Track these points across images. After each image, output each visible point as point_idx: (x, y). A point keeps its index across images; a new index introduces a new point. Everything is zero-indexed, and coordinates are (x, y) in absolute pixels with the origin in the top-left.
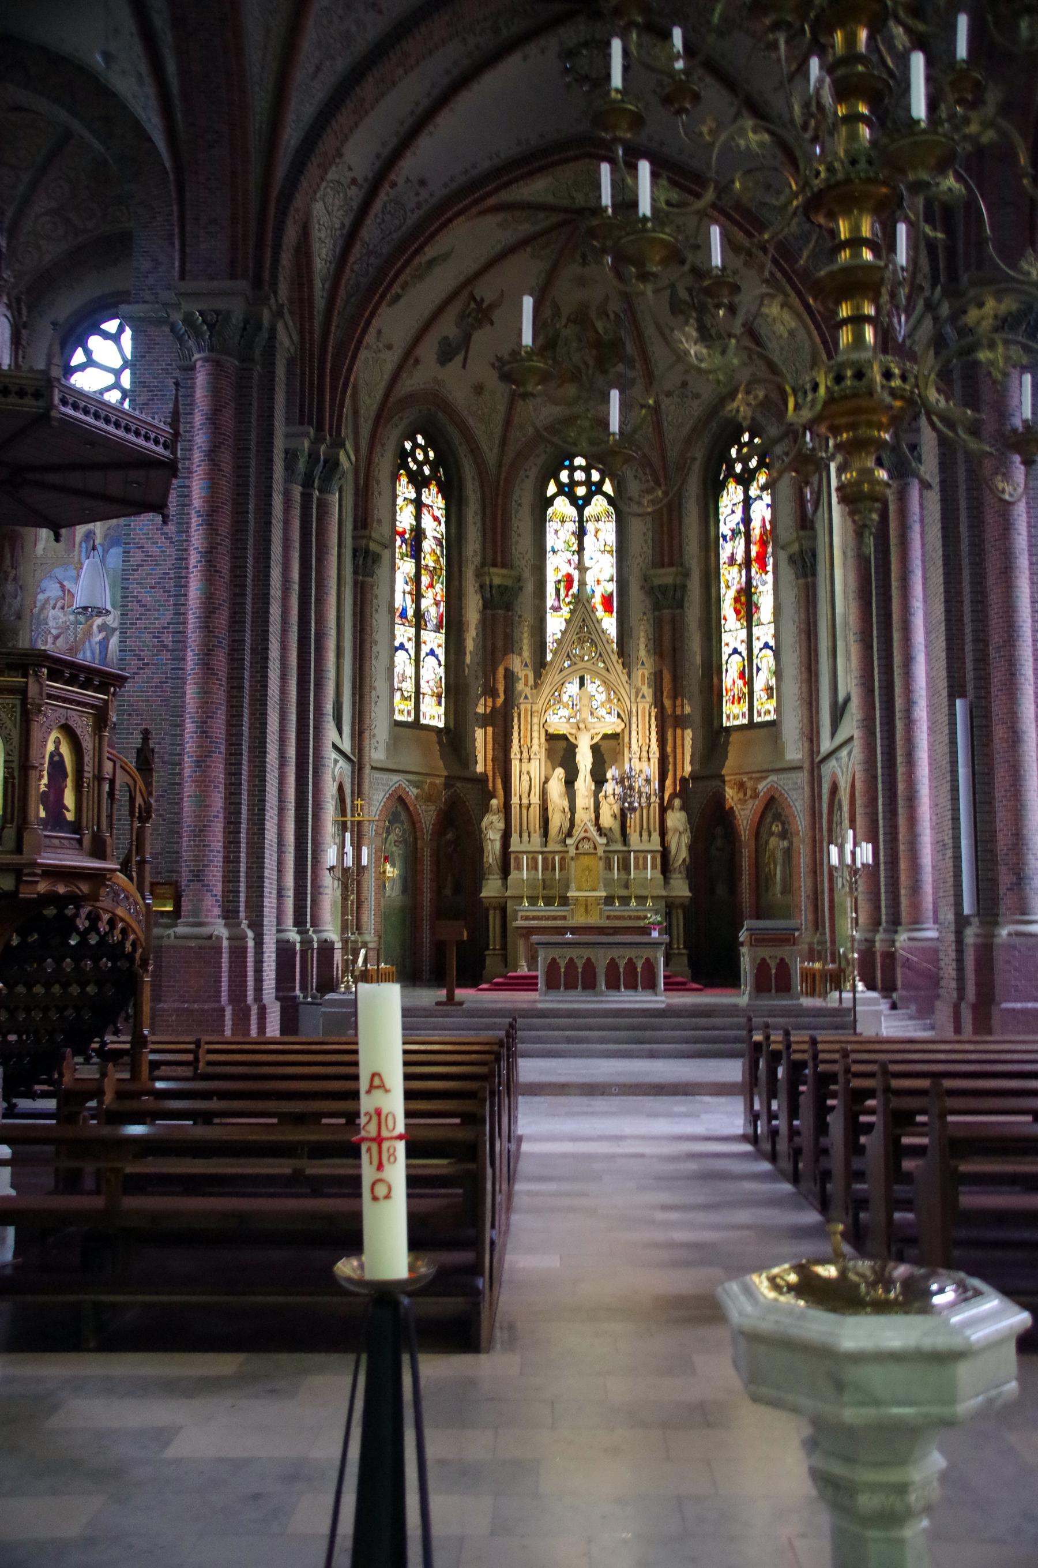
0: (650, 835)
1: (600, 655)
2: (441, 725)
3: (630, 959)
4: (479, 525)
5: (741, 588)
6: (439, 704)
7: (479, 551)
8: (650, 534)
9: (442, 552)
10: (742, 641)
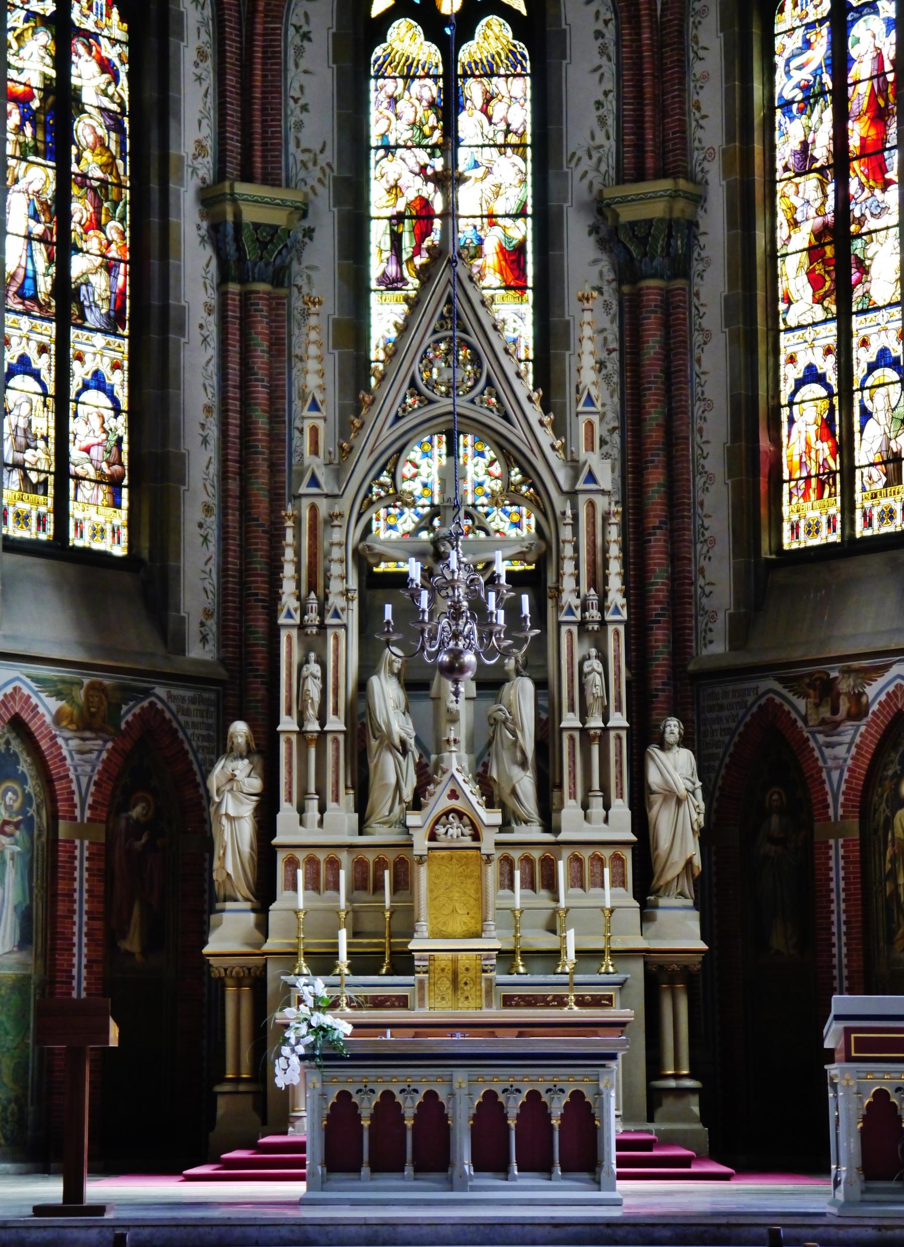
0: (607, 806)
1: (489, 383)
2: (120, 551)
3: (534, 1096)
4: (210, 81)
5: (825, 225)
6: (117, 505)
7: (209, 144)
8: (611, 104)
9: (121, 144)
10: (828, 351)
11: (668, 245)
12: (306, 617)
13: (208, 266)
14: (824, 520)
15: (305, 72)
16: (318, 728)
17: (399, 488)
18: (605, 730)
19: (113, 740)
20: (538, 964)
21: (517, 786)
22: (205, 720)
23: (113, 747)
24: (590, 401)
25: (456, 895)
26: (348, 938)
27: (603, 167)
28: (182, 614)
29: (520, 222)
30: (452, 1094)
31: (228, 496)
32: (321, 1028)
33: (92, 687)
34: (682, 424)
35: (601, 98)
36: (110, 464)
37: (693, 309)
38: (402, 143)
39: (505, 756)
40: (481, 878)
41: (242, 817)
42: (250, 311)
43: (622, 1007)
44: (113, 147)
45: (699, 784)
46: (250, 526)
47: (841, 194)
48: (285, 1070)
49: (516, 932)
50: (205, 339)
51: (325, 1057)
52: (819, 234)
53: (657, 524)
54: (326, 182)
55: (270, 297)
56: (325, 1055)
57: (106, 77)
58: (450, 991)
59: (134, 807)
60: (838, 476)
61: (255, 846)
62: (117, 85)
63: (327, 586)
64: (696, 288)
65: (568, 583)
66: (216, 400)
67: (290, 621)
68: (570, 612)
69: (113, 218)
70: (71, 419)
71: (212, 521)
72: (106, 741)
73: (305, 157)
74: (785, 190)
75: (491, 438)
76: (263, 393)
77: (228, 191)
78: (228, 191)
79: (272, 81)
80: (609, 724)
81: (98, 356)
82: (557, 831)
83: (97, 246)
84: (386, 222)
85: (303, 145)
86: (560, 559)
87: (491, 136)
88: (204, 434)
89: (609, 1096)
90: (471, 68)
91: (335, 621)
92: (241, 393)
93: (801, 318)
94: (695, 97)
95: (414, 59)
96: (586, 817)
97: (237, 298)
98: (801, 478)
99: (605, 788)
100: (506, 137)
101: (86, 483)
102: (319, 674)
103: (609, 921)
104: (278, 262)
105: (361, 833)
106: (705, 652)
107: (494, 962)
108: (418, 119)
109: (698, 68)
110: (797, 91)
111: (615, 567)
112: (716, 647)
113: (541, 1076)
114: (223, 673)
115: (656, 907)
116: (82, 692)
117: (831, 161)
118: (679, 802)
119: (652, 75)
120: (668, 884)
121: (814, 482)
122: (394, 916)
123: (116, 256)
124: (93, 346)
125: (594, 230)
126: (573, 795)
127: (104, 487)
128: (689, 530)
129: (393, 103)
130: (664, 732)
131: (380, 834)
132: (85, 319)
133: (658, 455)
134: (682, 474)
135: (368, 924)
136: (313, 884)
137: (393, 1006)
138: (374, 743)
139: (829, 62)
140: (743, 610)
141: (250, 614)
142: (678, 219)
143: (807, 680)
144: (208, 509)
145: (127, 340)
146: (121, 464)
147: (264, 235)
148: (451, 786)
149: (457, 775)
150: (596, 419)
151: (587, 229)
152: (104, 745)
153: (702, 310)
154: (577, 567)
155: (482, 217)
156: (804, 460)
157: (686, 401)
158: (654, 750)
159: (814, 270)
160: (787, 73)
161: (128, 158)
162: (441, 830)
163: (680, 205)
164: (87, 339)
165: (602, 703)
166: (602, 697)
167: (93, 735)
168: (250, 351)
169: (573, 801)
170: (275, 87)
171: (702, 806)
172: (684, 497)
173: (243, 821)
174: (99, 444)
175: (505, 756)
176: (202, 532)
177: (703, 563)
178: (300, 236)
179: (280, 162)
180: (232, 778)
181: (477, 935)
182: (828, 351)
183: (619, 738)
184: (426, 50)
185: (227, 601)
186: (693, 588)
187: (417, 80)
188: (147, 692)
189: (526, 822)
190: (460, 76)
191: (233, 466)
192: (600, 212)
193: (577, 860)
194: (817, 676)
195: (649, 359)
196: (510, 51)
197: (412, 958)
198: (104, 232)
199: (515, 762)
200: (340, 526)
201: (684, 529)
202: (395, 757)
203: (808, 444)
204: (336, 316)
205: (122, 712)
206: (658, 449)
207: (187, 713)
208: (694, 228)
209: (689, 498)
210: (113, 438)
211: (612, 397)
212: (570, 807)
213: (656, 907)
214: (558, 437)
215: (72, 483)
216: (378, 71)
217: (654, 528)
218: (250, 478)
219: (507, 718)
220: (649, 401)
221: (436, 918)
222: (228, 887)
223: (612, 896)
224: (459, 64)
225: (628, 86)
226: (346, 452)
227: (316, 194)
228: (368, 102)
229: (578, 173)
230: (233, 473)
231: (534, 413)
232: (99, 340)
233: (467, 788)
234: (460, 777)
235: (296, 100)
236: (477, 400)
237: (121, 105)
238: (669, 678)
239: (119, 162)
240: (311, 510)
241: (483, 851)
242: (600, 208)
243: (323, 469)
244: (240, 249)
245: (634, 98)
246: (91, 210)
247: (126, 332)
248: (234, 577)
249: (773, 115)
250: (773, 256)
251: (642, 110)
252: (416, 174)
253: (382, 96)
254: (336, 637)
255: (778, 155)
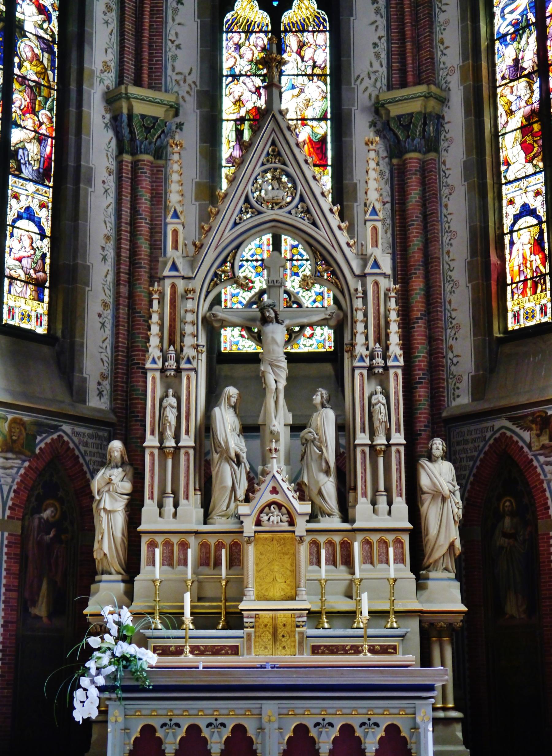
0: (390, 503)
1: (302, 199)
2: (41, 330)
3: (347, 729)
4: (114, 25)
5: (533, 111)
6: (41, 300)
7: (113, 65)
8: (383, 45)
9: (52, 61)
10: (537, 193)
11: (424, 130)
12: (166, 364)
13: (109, 143)
14: (538, 308)
15: (179, 24)
16: (174, 445)
17: (236, 274)
18: (389, 446)
19: (29, 461)
20: (338, 622)
21: (323, 488)
22: (100, 451)
23: (29, 466)
24: (374, 212)
25: (276, 568)
26: (191, 601)
27: (378, 85)
28: (85, 375)
29: (323, 123)
30: (261, 728)
31: (120, 296)
32: (124, 658)
33: (14, 421)
34: (435, 249)
35: (377, 41)
36: (36, 272)
37: (442, 173)
38: (244, 73)
39: (314, 467)
40: (295, 555)
41: (116, 511)
42: (138, 173)
43: (404, 654)
44: (46, 62)
45: (458, 487)
46: (135, 317)
47: (544, 87)
48: (83, 702)
49: (322, 597)
50: (106, 191)
51: (125, 689)
52: (528, 117)
53: (419, 316)
54: (192, 94)
55: (152, 165)
56: (127, 685)
57: (42, 17)
58: (271, 642)
59: (45, 510)
60: (548, 278)
61: (126, 534)
62: (50, 23)
63: (182, 341)
64: (443, 159)
65: (360, 339)
66: (113, 232)
67: (154, 366)
68: (362, 359)
69: (44, 108)
70: (8, 238)
71: (108, 314)
72: (23, 461)
73: (179, 77)
74: (503, 92)
75: (303, 239)
76: (146, 227)
77: (123, 91)
78: (123, 91)
79: (156, 28)
80: (391, 442)
81: (30, 198)
82: (353, 521)
83: (32, 125)
84: (233, 123)
85: (177, 71)
86: (354, 322)
87: (303, 69)
88: (104, 254)
89: (426, 730)
90: (290, 27)
91: (188, 366)
92: (131, 229)
93: (517, 174)
94: (440, 36)
95: (252, 21)
96: (374, 511)
97: (130, 165)
98: (520, 282)
99: (388, 490)
100: (313, 69)
101: (18, 282)
102: (175, 405)
103: (393, 588)
104: (158, 143)
105: (205, 523)
106: (454, 404)
107: (305, 619)
108: (254, 58)
109: (441, 18)
110: (510, 27)
111: (394, 328)
112: (462, 400)
113: (355, 709)
114: (112, 418)
115: (428, 579)
116: (6, 425)
117: (536, 68)
118: (444, 499)
119: (411, 23)
120: (436, 561)
121: (529, 283)
122: (229, 584)
123: (46, 133)
124: (26, 190)
125: (373, 124)
126: (365, 495)
127: (31, 286)
128: (441, 320)
129: (238, 48)
130: (431, 448)
131: (220, 524)
132: (21, 172)
133: (419, 269)
134: (436, 282)
135: (209, 592)
136: (168, 561)
137: (227, 654)
138: (216, 456)
139: (532, 5)
140: (481, 372)
141: (133, 377)
142: (431, 112)
143: (530, 418)
144: (105, 305)
145: (51, 189)
146: (44, 272)
147: (148, 123)
148: (272, 484)
149: (277, 475)
150: (379, 225)
151: (368, 124)
152: (22, 464)
153: (448, 172)
154: (366, 327)
155: (297, 120)
156: (521, 269)
157: (438, 234)
158: (424, 462)
159: (525, 141)
160: (503, 17)
161: (56, 71)
162: (264, 518)
163: (432, 104)
164: (22, 185)
165: (386, 426)
166: (386, 422)
167: (14, 456)
168: (137, 200)
169: (364, 499)
170: (158, 31)
171: (461, 503)
172: (437, 298)
173: (117, 514)
174: (28, 257)
175: (314, 467)
176: (101, 320)
177: (452, 342)
178: (174, 128)
179: (161, 80)
180: (109, 482)
181: (292, 598)
182: (537, 193)
183: (398, 452)
184: (260, 16)
185: (118, 368)
186: (444, 360)
187: (254, 35)
188: (56, 428)
189: (329, 515)
190: (283, 32)
191: (124, 277)
192: (377, 112)
193: (368, 543)
194: (538, 414)
195: (411, 205)
196: (316, 16)
197: (242, 617)
198: (38, 117)
199: (321, 470)
200: (193, 299)
201: (438, 319)
202: (231, 466)
203: (524, 258)
204: (198, 180)
205: (37, 441)
206: (419, 265)
207: (86, 444)
208: (441, 120)
209: (441, 299)
210: (39, 254)
211: (386, 233)
212: (363, 503)
213: (428, 579)
214: (352, 238)
215: (6, 281)
216: (228, 28)
217: (417, 318)
218: (135, 284)
219: (315, 438)
220: (412, 233)
221: (261, 585)
222: (105, 563)
223: (395, 570)
224: (282, 24)
225: (394, 32)
226: (199, 247)
227: (185, 101)
228: (221, 47)
229: (362, 87)
230: (124, 281)
231: (334, 220)
232: (31, 187)
233: (285, 486)
234: (279, 477)
235: (173, 42)
236: (293, 212)
237: (53, 36)
238: (428, 422)
239: (50, 73)
240: (172, 287)
241: (297, 534)
242: (378, 108)
243: (181, 260)
244: (132, 132)
245: (399, 40)
246: (28, 100)
247: (51, 184)
248: (123, 352)
249: (494, 44)
250: (496, 135)
251: (405, 47)
252: (253, 93)
253: (231, 44)
254: (188, 378)
255: (498, 70)
